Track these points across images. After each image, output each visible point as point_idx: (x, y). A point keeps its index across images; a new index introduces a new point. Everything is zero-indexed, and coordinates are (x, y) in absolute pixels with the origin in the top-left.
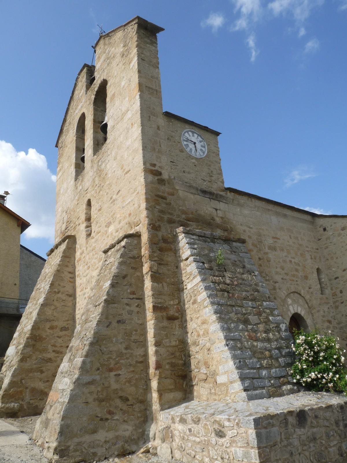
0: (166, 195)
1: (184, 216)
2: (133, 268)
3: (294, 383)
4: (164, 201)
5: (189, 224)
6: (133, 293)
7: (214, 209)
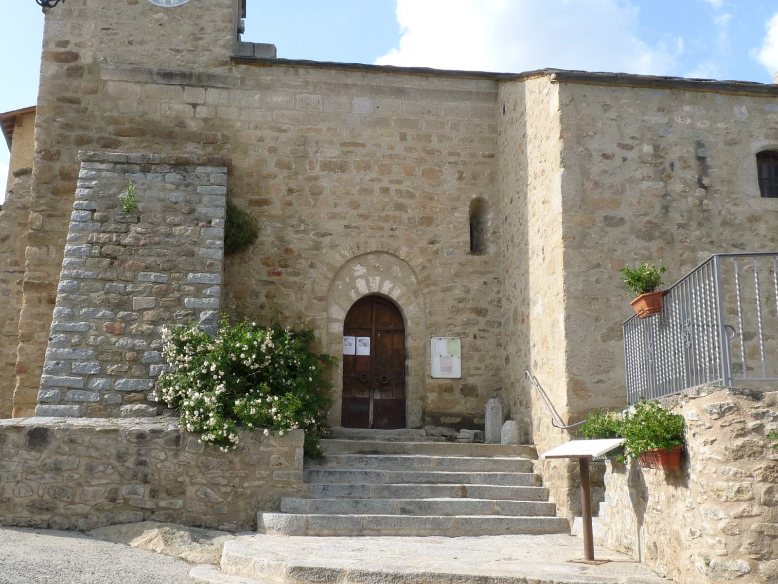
0: (79, 95)
1: (111, 128)
2: (20, 224)
3: (155, 402)
4: (75, 106)
5: (120, 142)
6: (16, 263)
7: (188, 106)
